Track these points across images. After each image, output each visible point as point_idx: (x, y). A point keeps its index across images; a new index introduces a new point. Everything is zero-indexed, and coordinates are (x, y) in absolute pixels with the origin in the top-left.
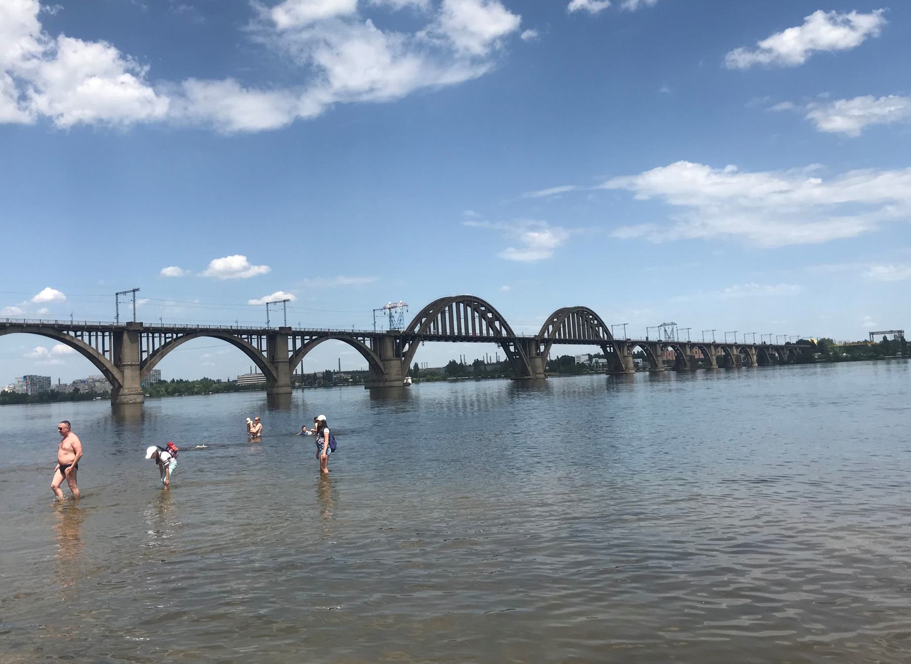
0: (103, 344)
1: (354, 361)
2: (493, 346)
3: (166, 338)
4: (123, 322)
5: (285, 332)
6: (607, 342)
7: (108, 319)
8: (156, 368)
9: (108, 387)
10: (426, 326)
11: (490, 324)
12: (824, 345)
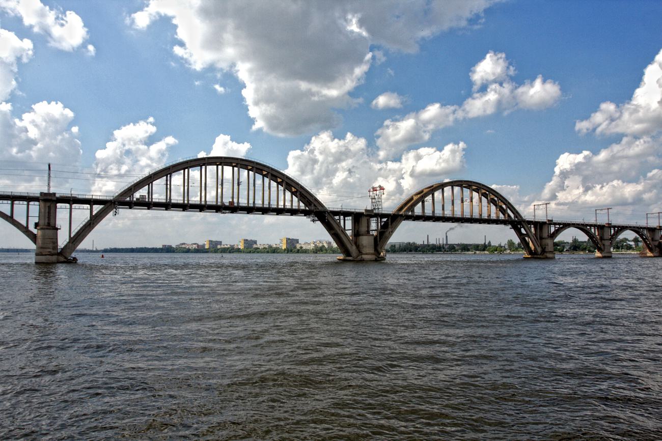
10: (412, 208)
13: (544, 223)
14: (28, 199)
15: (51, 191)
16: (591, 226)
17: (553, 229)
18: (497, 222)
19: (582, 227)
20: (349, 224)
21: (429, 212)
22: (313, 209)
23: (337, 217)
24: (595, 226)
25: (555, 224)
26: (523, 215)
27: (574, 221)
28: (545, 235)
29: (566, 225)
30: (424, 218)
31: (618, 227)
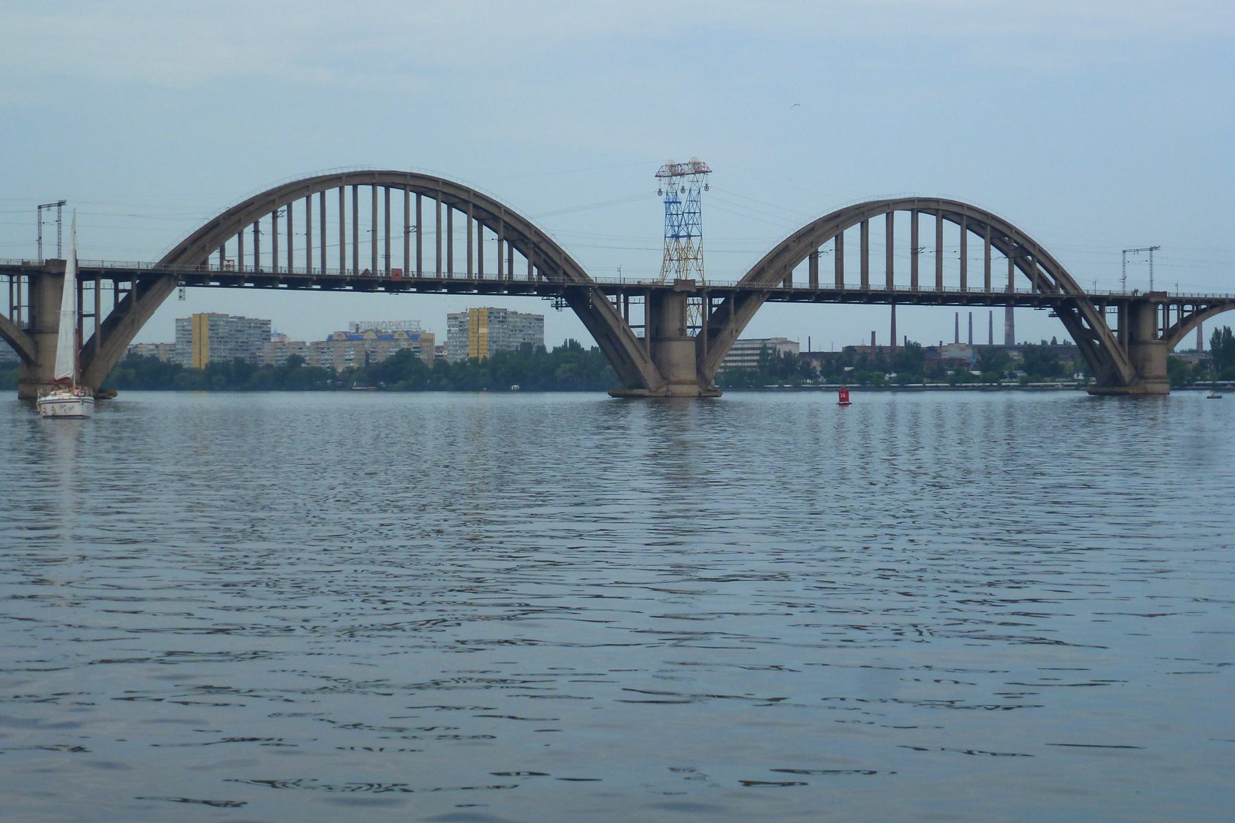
3: (117, 291)
21: (827, 280)
22: (560, 279)
23: (612, 298)
31: (1195, 302)
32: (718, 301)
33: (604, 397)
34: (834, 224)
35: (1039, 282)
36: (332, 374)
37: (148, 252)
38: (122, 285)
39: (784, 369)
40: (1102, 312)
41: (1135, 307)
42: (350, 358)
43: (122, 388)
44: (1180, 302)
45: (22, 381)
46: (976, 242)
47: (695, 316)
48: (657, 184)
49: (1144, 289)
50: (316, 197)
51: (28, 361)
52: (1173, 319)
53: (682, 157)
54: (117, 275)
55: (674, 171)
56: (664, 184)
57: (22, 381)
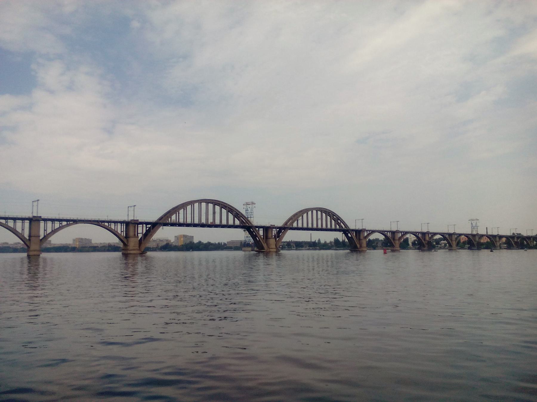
0: (120, 229)
1: (382, 237)
2: (241, 231)
3: (146, 227)
4: (131, 218)
5: (397, 232)
6: (346, 231)
7: (125, 218)
8: (49, 239)
9: (26, 247)
11: (337, 223)
12: (209, 244)
13: (426, 233)
14: (23, 219)
15: (39, 215)
16: (387, 232)
17: (366, 234)
18: (234, 226)
19: (382, 232)
20: (261, 232)
21: (300, 225)
23: (257, 229)
24: (390, 232)
25: (367, 231)
26: (253, 223)
27: (377, 229)
28: (362, 237)
29: (373, 232)
30: (173, 225)
31: (433, 233)
32: (150, 226)
33: (348, 251)
34: (184, 206)
35: (242, 222)
36: (150, 248)
37: (154, 218)
38: (148, 226)
39: (289, 245)
40: (259, 230)
41: (358, 232)
42: (181, 243)
43: (148, 251)
44: (401, 232)
45: (123, 250)
46: (224, 211)
47: (274, 232)
48: (243, 206)
49: (361, 228)
50: (305, 215)
51: (125, 244)
52: (400, 235)
53: (249, 200)
54: (147, 223)
55: (247, 204)
56: (245, 207)
57: (123, 250)
